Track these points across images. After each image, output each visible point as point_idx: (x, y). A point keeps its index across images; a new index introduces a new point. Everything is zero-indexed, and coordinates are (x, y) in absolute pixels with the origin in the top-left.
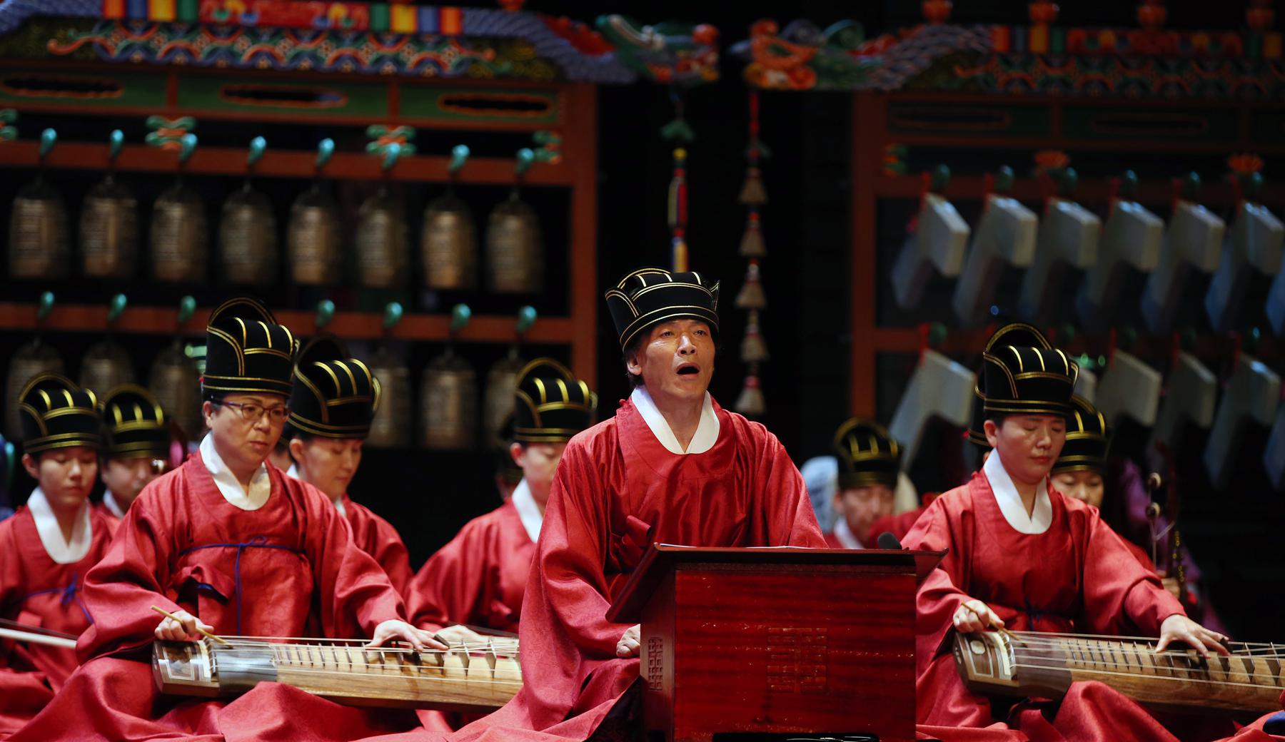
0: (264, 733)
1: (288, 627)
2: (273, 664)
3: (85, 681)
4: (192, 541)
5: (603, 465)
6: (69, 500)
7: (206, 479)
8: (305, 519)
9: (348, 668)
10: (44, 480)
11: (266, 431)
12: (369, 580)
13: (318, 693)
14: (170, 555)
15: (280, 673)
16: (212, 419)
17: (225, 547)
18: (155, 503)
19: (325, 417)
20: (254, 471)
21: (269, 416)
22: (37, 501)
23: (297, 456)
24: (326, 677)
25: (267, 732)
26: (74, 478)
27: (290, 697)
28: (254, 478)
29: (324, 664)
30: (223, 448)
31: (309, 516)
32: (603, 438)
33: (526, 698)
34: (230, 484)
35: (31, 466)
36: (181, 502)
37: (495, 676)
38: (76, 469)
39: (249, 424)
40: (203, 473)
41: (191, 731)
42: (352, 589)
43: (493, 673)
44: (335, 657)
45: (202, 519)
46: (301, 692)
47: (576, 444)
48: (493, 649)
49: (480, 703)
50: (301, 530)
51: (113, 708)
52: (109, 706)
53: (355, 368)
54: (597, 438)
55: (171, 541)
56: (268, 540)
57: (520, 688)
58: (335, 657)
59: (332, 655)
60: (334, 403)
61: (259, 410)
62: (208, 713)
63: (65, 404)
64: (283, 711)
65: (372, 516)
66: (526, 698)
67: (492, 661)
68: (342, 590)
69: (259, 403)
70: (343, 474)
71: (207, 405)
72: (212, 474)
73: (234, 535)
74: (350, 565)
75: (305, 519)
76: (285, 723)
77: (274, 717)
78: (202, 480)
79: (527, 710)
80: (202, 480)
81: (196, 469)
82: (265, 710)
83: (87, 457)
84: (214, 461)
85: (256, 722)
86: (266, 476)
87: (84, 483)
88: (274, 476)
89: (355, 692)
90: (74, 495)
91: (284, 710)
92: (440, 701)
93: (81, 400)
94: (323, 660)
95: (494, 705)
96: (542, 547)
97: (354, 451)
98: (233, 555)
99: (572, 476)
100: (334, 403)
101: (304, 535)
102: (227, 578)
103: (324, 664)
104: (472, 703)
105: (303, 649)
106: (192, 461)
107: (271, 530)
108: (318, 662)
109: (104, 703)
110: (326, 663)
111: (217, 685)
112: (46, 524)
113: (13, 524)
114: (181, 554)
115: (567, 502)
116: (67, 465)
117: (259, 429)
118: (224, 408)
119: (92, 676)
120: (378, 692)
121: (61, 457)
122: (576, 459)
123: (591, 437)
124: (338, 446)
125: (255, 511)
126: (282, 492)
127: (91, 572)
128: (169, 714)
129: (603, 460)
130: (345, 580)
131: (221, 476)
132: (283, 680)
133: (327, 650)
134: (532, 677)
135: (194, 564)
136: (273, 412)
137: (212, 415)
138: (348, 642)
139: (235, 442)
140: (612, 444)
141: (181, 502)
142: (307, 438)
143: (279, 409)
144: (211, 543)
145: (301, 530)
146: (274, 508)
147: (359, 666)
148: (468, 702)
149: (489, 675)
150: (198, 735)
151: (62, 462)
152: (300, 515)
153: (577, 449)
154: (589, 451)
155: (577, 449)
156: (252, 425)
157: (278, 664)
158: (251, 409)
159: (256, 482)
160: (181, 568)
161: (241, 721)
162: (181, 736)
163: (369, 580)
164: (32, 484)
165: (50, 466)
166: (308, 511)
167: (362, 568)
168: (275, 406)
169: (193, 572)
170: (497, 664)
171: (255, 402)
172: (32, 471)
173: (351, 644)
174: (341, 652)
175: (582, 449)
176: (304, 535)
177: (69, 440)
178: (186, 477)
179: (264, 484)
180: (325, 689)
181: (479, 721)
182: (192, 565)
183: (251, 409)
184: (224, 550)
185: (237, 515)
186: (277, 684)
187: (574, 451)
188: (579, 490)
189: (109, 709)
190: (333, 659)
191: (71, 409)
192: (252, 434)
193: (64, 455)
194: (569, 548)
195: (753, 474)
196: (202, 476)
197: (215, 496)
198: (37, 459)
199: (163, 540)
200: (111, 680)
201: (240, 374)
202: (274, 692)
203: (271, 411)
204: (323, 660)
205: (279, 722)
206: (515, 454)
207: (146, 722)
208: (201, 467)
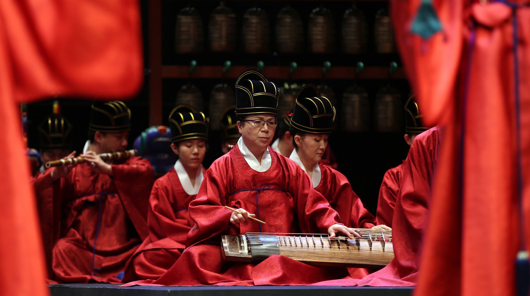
0: (273, 279)
1: (285, 227)
2: (278, 246)
3: (189, 255)
4: (235, 188)
5: (431, 150)
6: (193, 165)
7: (240, 158)
8: (289, 175)
9: (313, 248)
10: (181, 156)
11: (267, 132)
12: (321, 206)
13: (299, 260)
14: (226, 194)
15: (281, 251)
16: (241, 129)
17: (251, 191)
18: (218, 170)
19: (312, 123)
20: (263, 152)
21: (267, 124)
22: (178, 166)
23: (298, 143)
24: (303, 252)
25: (274, 279)
26: (195, 154)
27: (285, 261)
28: (263, 156)
29: (302, 246)
30: (249, 143)
31: (291, 174)
32: (432, 138)
33: (395, 263)
34: (252, 159)
35: (175, 149)
36: (230, 169)
37: (385, 251)
38: (196, 150)
39: (259, 128)
40: (239, 155)
41: (239, 279)
42: (313, 210)
43: (384, 249)
44: (307, 242)
45: (241, 177)
46: (291, 259)
47: (418, 140)
48: (384, 238)
49: (378, 264)
50: (287, 181)
51: (202, 268)
52: (200, 267)
53: (323, 100)
54: (428, 138)
55: (226, 188)
56: (271, 186)
57: (393, 258)
58: (307, 242)
59: (306, 241)
60: (315, 117)
61: (262, 122)
62: (247, 269)
63: (191, 119)
64: (282, 269)
65: (333, 171)
66: (395, 263)
67: (383, 244)
68: (309, 211)
69: (262, 119)
70: (320, 152)
71: (238, 122)
72: (243, 155)
73: (255, 185)
74: (311, 199)
75: (289, 175)
76: (283, 274)
77: (278, 271)
78: (239, 158)
79: (396, 269)
80: (239, 158)
81: (236, 153)
82: (273, 268)
83: (201, 144)
84: (244, 149)
85: (269, 274)
86: (269, 155)
87: (200, 156)
88: (273, 155)
89: (317, 259)
90: (195, 162)
91: (283, 268)
92: (358, 263)
93: (198, 117)
94: (301, 244)
95: (384, 265)
96: (402, 191)
97: (325, 140)
98: (255, 195)
99: (416, 156)
100: (315, 117)
101: (288, 183)
102: (252, 206)
103: (302, 246)
104: (374, 264)
105: (292, 238)
106: (234, 149)
107: (272, 182)
108: (299, 245)
109: (198, 266)
110: (303, 245)
111: (250, 256)
112: (183, 177)
113: (168, 176)
114: (230, 195)
115: (413, 169)
116: (192, 148)
117: (263, 131)
118: (246, 123)
119: (193, 253)
120: (328, 259)
121: (189, 144)
122: (418, 147)
123: (425, 137)
124: (318, 138)
125: (264, 172)
126: (277, 163)
127: (193, 202)
128: (229, 270)
129: (431, 148)
130: (309, 206)
131: (248, 156)
132: (282, 254)
133: (304, 239)
134: (399, 252)
135: (237, 200)
136: (269, 123)
137: (241, 127)
138: (314, 235)
139: (253, 137)
140: (435, 140)
141: (230, 169)
142: (303, 134)
143: (272, 121)
144: (244, 189)
145: (287, 181)
146: (274, 170)
147: (318, 247)
148: (372, 264)
149: (382, 250)
150: (242, 281)
151: (189, 147)
152: (286, 173)
153: (419, 143)
154: (424, 143)
155: (419, 143)
156: (260, 130)
157: (280, 246)
158: (258, 122)
159: (265, 158)
160: (231, 202)
161: (262, 273)
162: (234, 281)
163: (321, 206)
164: (174, 158)
165: (184, 148)
166: (290, 171)
167: (318, 200)
168: (270, 120)
169: (236, 204)
170: (385, 245)
171: (260, 118)
172: (175, 151)
173: (315, 236)
174: (310, 240)
175: (421, 142)
176: (288, 183)
177: (193, 136)
178: (232, 157)
179: (268, 160)
180: (303, 258)
181: (373, 274)
182: (236, 200)
183: (258, 122)
184: (250, 192)
185: (256, 175)
186: (279, 256)
187: (417, 144)
188: (420, 163)
189: (200, 268)
190: (306, 243)
191: (193, 122)
192: (261, 134)
193: (190, 143)
194: (415, 191)
195: (339, 258)
196: (239, 157)
197: (245, 166)
198: (177, 145)
199: (222, 188)
200: (202, 255)
201: (252, 106)
202: (278, 259)
203: (269, 122)
204: (301, 244)
205: (280, 274)
206: (406, 139)
207: (218, 275)
208: (238, 152)
